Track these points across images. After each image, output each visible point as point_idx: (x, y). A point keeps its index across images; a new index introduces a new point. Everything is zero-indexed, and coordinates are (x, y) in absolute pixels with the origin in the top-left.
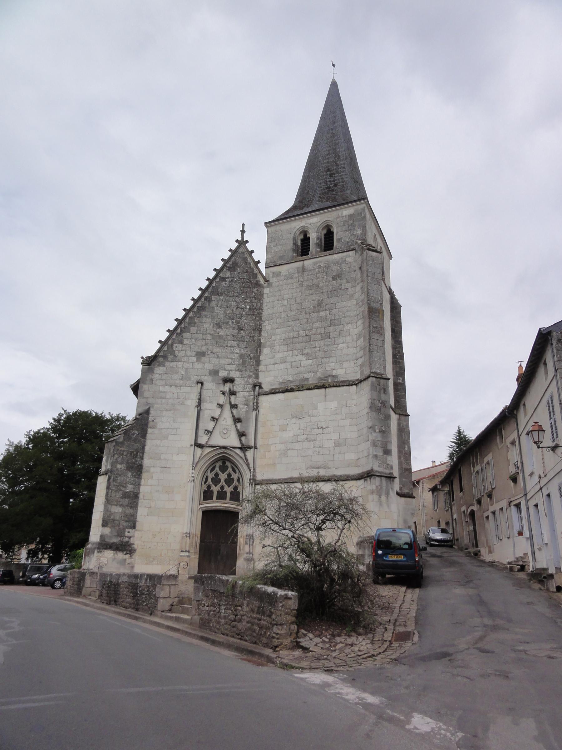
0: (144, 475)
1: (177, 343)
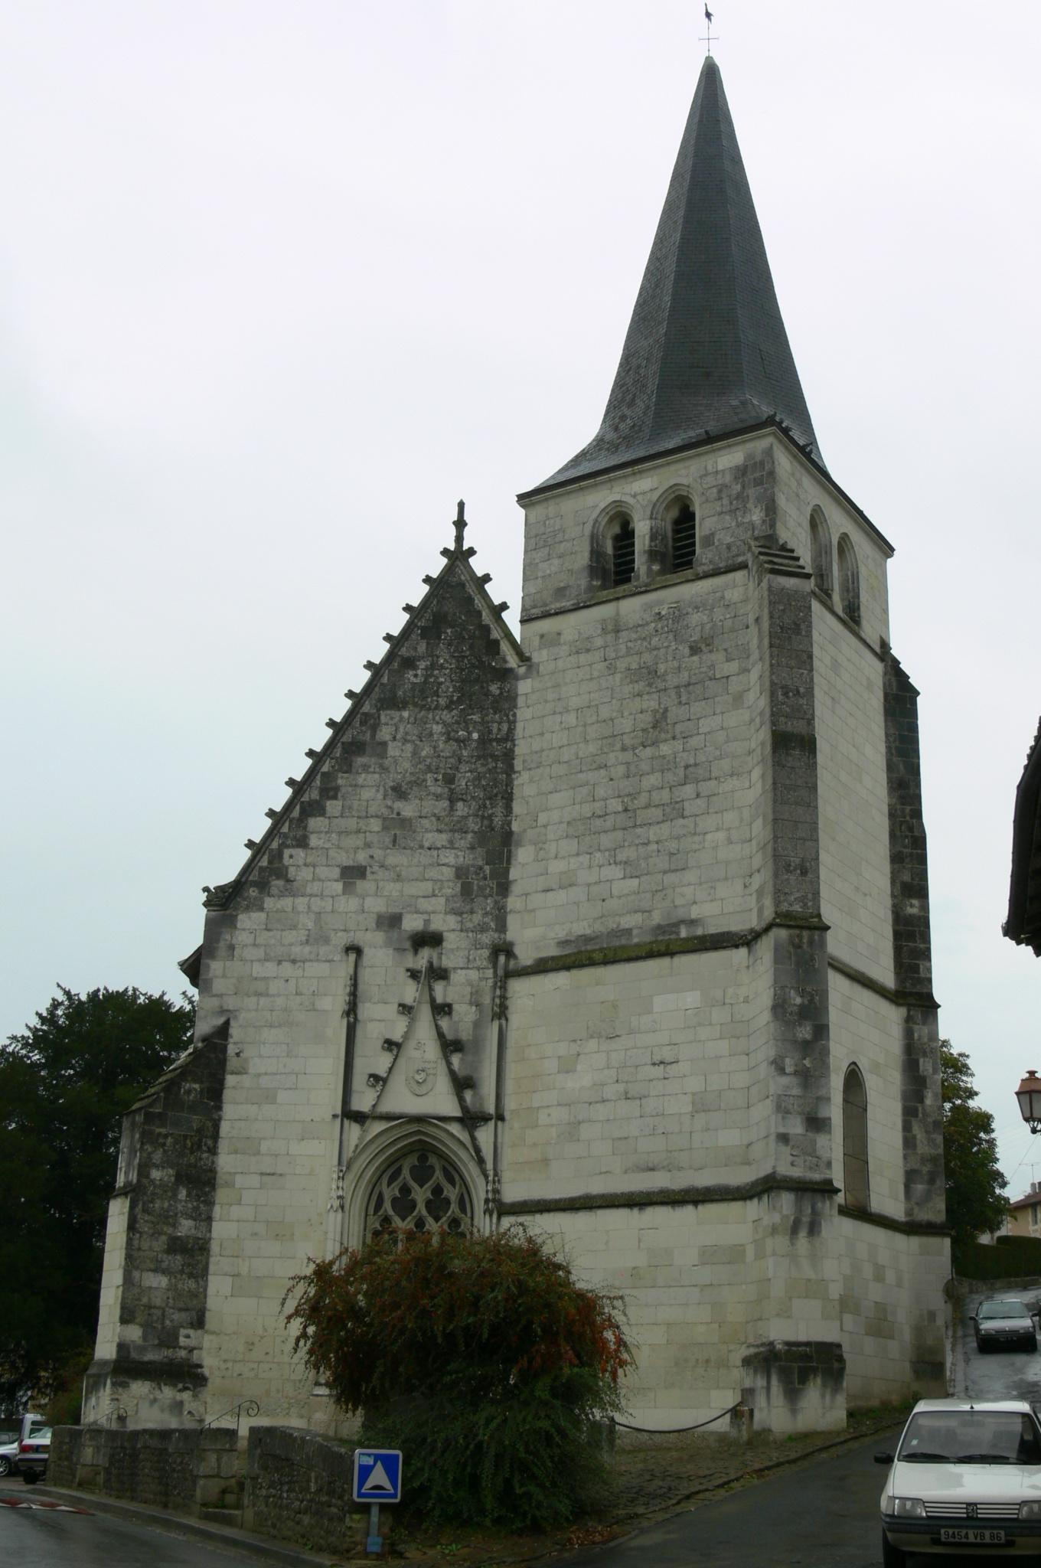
0: (221, 1195)
1: (293, 847)
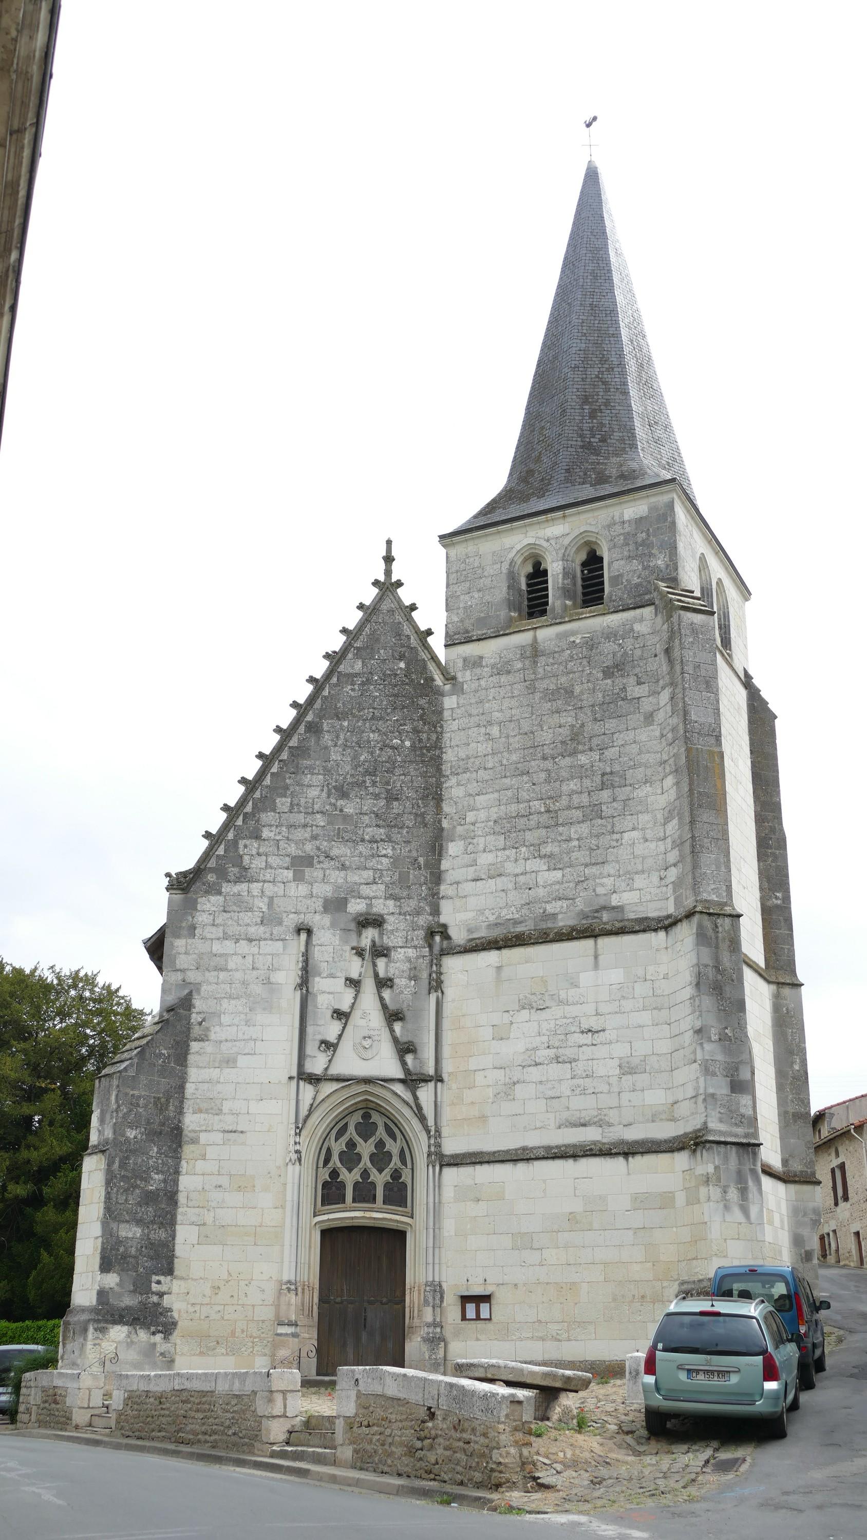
0: (188, 1151)
